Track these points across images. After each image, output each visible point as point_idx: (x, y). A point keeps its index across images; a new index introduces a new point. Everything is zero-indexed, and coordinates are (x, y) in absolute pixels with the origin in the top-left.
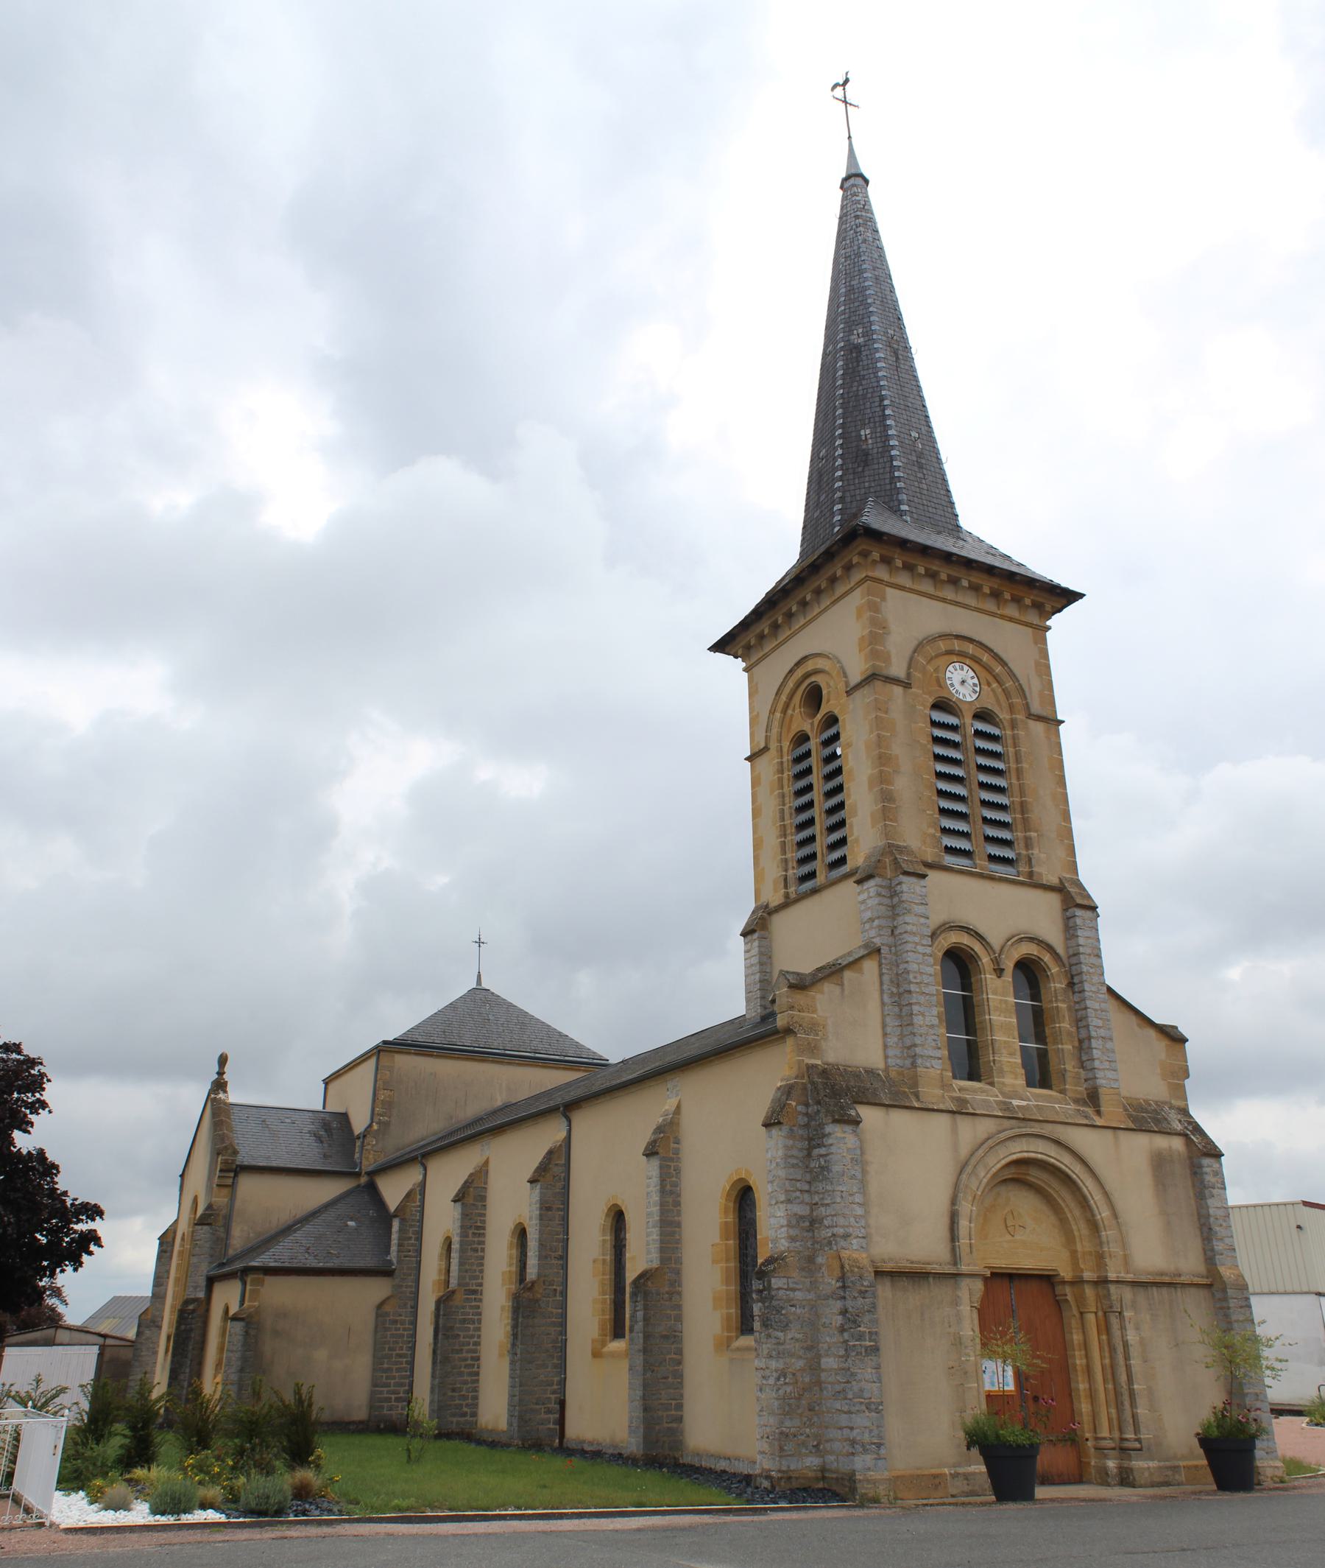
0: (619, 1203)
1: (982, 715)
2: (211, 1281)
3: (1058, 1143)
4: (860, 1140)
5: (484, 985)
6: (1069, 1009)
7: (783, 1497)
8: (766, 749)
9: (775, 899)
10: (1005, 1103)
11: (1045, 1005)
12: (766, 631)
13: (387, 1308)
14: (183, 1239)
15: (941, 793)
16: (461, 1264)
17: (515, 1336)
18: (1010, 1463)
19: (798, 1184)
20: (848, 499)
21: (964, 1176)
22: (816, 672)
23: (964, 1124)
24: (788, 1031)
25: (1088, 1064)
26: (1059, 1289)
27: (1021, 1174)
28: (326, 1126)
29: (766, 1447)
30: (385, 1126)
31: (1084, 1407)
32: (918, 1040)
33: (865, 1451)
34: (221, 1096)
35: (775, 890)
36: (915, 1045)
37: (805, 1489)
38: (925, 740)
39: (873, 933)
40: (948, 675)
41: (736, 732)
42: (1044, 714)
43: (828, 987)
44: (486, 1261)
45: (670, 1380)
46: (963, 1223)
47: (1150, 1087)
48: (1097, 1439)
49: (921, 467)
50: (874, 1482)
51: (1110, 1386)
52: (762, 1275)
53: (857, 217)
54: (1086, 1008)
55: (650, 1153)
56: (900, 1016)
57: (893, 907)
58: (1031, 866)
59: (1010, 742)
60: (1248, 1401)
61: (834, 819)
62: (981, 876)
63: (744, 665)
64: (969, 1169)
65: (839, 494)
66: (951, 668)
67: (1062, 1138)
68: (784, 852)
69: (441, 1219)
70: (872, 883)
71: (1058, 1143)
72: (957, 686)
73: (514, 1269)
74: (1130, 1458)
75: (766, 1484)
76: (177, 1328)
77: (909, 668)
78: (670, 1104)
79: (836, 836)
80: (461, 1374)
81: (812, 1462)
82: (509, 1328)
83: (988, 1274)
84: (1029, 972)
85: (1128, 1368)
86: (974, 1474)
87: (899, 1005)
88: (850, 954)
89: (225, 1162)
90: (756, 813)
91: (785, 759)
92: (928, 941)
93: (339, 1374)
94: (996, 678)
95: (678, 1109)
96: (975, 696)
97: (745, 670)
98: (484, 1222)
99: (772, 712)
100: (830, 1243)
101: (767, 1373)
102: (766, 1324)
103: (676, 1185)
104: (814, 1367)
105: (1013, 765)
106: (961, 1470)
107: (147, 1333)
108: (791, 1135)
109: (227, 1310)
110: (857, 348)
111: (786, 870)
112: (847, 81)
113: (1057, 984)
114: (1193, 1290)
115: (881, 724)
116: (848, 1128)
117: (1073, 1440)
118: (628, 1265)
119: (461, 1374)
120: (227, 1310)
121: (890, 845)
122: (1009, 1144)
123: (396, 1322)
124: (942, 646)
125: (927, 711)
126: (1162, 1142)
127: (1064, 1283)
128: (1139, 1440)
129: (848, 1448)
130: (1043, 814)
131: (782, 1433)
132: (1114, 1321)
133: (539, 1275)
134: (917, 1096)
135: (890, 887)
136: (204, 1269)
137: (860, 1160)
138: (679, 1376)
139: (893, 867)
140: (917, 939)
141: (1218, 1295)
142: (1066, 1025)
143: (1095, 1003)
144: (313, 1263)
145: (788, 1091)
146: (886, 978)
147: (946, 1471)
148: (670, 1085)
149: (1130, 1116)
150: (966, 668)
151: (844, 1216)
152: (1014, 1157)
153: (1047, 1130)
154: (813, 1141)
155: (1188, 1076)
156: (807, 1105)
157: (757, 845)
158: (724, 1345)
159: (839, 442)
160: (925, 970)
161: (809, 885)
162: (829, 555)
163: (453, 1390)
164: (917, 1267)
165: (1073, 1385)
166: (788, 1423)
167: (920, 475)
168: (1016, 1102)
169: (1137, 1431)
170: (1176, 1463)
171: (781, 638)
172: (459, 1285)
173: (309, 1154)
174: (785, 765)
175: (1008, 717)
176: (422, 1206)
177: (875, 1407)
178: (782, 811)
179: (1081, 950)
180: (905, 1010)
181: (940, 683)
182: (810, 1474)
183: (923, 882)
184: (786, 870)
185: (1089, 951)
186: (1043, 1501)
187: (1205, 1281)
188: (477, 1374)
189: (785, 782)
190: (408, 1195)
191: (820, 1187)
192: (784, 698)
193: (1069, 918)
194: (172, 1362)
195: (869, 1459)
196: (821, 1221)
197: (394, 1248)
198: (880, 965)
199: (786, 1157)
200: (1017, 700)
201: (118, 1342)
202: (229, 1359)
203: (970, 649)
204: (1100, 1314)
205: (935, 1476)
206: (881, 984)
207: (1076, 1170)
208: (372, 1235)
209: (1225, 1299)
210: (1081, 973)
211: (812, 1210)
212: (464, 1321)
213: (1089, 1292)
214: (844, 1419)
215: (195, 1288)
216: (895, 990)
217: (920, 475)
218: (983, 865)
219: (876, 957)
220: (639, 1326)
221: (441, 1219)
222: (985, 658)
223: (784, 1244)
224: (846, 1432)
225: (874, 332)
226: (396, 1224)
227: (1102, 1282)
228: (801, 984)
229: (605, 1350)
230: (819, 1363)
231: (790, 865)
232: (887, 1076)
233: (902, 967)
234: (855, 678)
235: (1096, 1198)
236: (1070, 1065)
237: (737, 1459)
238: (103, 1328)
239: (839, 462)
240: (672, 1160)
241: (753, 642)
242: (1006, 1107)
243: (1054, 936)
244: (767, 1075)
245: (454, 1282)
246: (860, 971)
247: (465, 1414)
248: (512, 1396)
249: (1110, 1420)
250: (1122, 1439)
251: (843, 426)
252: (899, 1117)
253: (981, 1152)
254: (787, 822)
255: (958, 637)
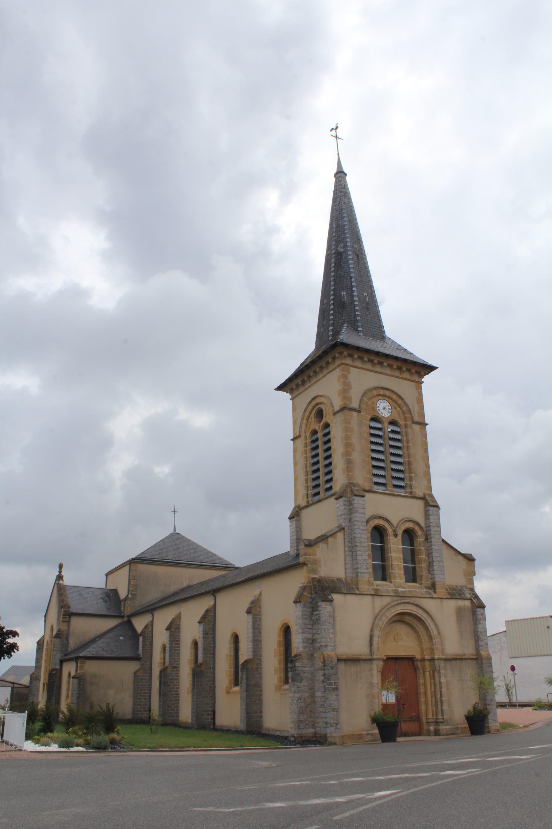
0: (237, 632)
1: (393, 423)
2: (62, 662)
3: (417, 605)
4: (333, 608)
5: (177, 531)
6: (425, 549)
7: (299, 743)
8: (299, 436)
9: (303, 503)
10: (395, 590)
11: (415, 548)
12: (300, 383)
13: (138, 674)
14: (47, 643)
15: (374, 459)
16: (170, 656)
17: (193, 685)
18: (388, 728)
19: (307, 626)
20: (336, 325)
21: (376, 620)
22: (321, 403)
23: (378, 600)
24: (304, 564)
25: (432, 572)
26: (416, 663)
27: (401, 618)
28: (108, 595)
29: (292, 726)
30: (134, 595)
31: (423, 707)
32: (359, 566)
33: (331, 726)
34: (61, 582)
35: (303, 499)
36: (358, 568)
37: (308, 741)
38: (366, 435)
39: (342, 521)
40: (378, 405)
41: (287, 429)
42: (420, 421)
43: (322, 545)
44: (181, 655)
45: (257, 702)
46: (375, 639)
47: (458, 580)
48: (427, 719)
49: (368, 309)
50: (335, 737)
51: (434, 699)
52: (292, 661)
53: (341, 192)
54: (432, 549)
55: (249, 612)
56: (352, 556)
57: (350, 510)
58: (411, 489)
59: (404, 434)
60: (487, 702)
61: (328, 469)
62: (389, 494)
63: (290, 397)
64: (379, 618)
65: (331, 322)
66: (379, 402)
67: (418, 603)
68: (307, 483)
69: (161, 637)
70: (341, 499)
71: (417, 605)
72: (382, 410)
73: (193, 658)
74: (439, 725)
75: (293, 739)
76: (49, 681)
77: (360, 403)
78: (257, 592)
79: (328, 477)
80: (172, 700)
81: (311, 731)
82: (191, 682)
83: (385, 658)
84: (409, 535)
85: (441, 692)
86: (375, 733)
87: (352, 551)
88: (331, 530)
89: (65, 611)
90: (295, 464)
91: (308, 441)
92: (365, 524)
93: (123, 703)
94: (399, 406)
95: (260, 594)
96: (389, 415)
97: (291, 399)
98: (179, 638)
99: (302, 420)
100: (319, 649)
101: (294, 698)
102: (293, 680)
103: (259, 625)
104: (313, 696)
105: (405, 444)
106: (369, 732)
107: (34, 682)
108: (305, 606)
109: (70, 674)
110: (341, 253)
111: (308, 491)
112: (337, 128)
113: (420, 539)
114: (470, 661)
115: (347, 429)
116: (328, 603)
117: (418, 719)
118: (240, 657)
119: (172, 700)
120: (70, 674)
121: (350, 483)
122: (396, 607)
123: (143, 679)
124: (375, 392)
125: (368, 422)
126: (461, 603)
127: (417, 660)
128: (443, 719)
129: (325, 725)
130: (418, 467)
131: (299, 721)
132: (436, 674)
133: (203, 661)
134: (358, 589)
135: (349, 501)
136: (59, 656)
137: (333, 616)
138: (261, 700)
139: (351, 492)
140: (360, 523)
141: (480, 662)
142: (423, 556)
143: (436, 546)
144: (105, 654)
145: (304, 588)
146: (346, 540)
147: (364, 733)
148: (257, 584)
149: (448, 593)
150: (386, 402)
151: (326, 638)
152: (398, 612)
153: (412, 600)
154: (314, 608)
155: (475, 575)
156: (311, 594)
157: (296, 479)
158: (278, 688)
159: (332, 297)
160: (363, 536)
161: (317, 498)
162: (326, 353)
163: (169, 707)
164: (356, 657)
165: (419, 699)
166: (301, 717)
167: (367, 313)
168: (400, 590)
169: (442, 715)
170: (457, 726)
171: (306, 387)
172: (169, 664)
173: (100, 607)
174: (308, 444)
175: (404, 423)
176: (152, 631)
177: (336, 710)
178: (306, 465)
179: (431, 524)
180: (354, 554)
181: (374, 409)
182: (311, 735)
183: (363, 499)
184: (308, 491)
185: (434, 525)
186: (399, 742)
187: (476, 657)
188: (178, 700)
189: (308, 451)
190: (146, 626)
191: (316, 626)
192: (307, 413)
193: (427, 511)
194: (48, 695)
195: (333, 729)
196: (316, 640)
197: (140, 648)
198: (344, 534)
199: (303, 615)
200: (408, 415)
201: (19, 686)
202: (72, 694)
203: (388, 393)
204: (431, 672)
205: (359, 735)
206: (345, 542)
207: (424, 616)
208: (131, 644)
209: (482, 664)
210: (430, 534)
211: (313, 636)
212: (172, 679)
213: (427, 663)
214: (323, 715)
215: (55, 664)
216: (350, 545)
217: (367, 313)
218: (390, 488)
219: (342, 531)
220: (244, 681)
221: (161, 637)
222: (394, 397)
223: (301, 649)
224: (324, 719)
225: (348, 246)
226: (141, 639)
227: (432, 660)
228: (310, 544)
229: (231, 690)
230: (315, 694)
231: (309, 488)
232: (346, 581)
233: (353, 535)
234: (337, 408)
235: (432, 627)
236: (425, 573)
237: (283, 731)
238: (10, 679)
239: (332, 307)
240: (257, 615)
241: (294, 387)
242: (396, 592)
243: (421, 520)
244: (296, 581)
245: (167, 663)
246: (336, 538)
247: (173, 716)
248: (193, 709)
249: (433, 711)
250: (437, 719)
251: (334, 290)
252: (350, 598)
253: (384, 611)
254: (308, 469)
255: (382, 388)
